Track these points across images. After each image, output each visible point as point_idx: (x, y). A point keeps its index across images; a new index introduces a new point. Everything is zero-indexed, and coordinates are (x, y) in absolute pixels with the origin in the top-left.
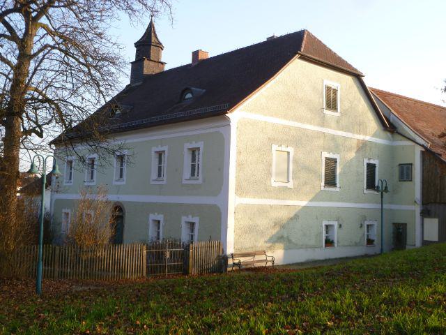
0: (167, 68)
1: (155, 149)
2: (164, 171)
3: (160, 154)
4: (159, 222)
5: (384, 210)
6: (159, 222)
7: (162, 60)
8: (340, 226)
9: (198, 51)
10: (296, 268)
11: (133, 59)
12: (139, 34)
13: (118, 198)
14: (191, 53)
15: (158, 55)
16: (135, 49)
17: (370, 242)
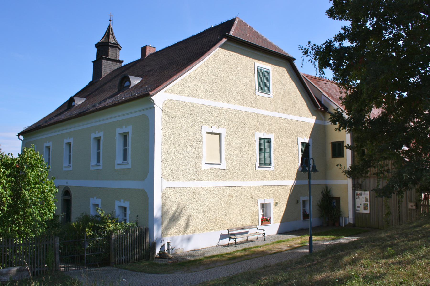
0: (123, 64)
1: (93, 135)
2: (221, 170)
3: (98, 140)
4: (125, 208)
5: (311, 187)
6: (125, 208)
7: (121, 59)
8: (276, 204)
9: (146, 46)
10: (289, 251)
11: (95, 59)
12: (99, 38)
13: (67, 183)
14: (141, 49)
15: (116, 55)
16: (96, 49)
17: (306, 216)
